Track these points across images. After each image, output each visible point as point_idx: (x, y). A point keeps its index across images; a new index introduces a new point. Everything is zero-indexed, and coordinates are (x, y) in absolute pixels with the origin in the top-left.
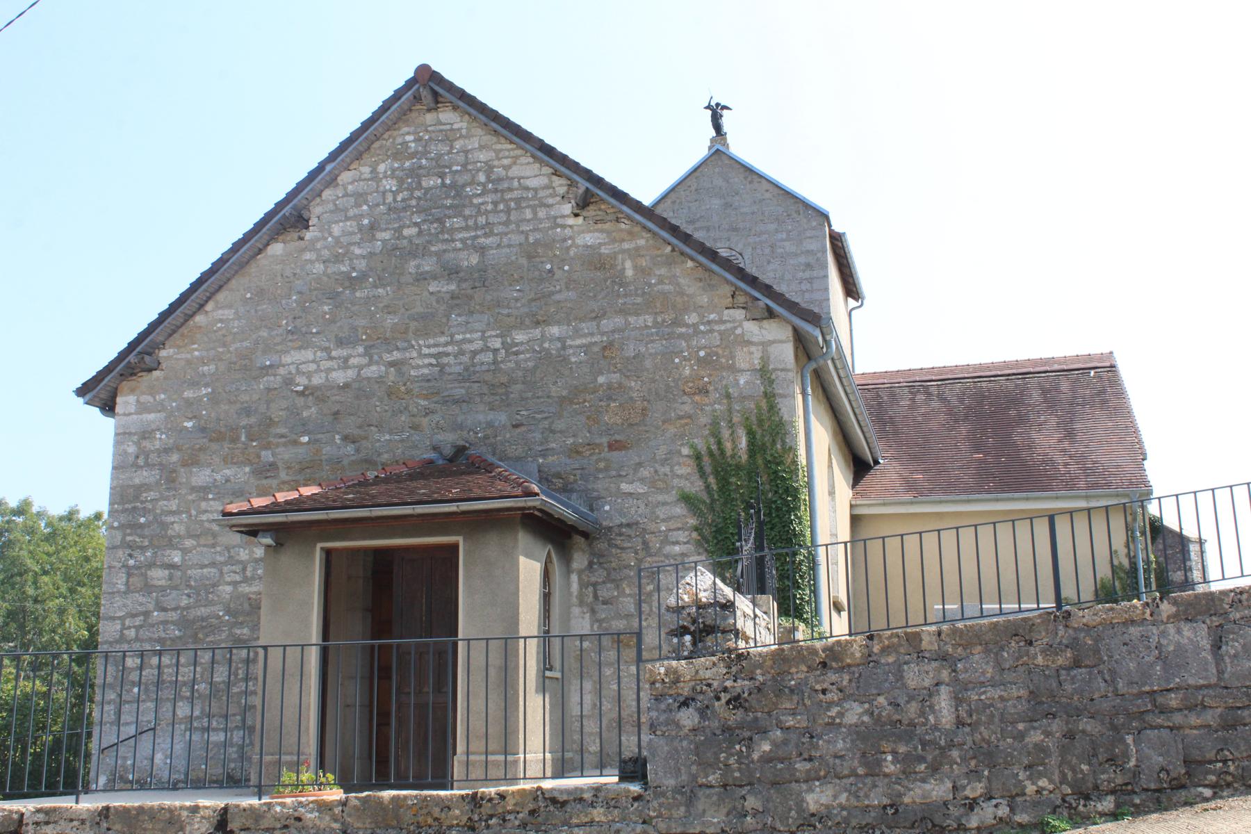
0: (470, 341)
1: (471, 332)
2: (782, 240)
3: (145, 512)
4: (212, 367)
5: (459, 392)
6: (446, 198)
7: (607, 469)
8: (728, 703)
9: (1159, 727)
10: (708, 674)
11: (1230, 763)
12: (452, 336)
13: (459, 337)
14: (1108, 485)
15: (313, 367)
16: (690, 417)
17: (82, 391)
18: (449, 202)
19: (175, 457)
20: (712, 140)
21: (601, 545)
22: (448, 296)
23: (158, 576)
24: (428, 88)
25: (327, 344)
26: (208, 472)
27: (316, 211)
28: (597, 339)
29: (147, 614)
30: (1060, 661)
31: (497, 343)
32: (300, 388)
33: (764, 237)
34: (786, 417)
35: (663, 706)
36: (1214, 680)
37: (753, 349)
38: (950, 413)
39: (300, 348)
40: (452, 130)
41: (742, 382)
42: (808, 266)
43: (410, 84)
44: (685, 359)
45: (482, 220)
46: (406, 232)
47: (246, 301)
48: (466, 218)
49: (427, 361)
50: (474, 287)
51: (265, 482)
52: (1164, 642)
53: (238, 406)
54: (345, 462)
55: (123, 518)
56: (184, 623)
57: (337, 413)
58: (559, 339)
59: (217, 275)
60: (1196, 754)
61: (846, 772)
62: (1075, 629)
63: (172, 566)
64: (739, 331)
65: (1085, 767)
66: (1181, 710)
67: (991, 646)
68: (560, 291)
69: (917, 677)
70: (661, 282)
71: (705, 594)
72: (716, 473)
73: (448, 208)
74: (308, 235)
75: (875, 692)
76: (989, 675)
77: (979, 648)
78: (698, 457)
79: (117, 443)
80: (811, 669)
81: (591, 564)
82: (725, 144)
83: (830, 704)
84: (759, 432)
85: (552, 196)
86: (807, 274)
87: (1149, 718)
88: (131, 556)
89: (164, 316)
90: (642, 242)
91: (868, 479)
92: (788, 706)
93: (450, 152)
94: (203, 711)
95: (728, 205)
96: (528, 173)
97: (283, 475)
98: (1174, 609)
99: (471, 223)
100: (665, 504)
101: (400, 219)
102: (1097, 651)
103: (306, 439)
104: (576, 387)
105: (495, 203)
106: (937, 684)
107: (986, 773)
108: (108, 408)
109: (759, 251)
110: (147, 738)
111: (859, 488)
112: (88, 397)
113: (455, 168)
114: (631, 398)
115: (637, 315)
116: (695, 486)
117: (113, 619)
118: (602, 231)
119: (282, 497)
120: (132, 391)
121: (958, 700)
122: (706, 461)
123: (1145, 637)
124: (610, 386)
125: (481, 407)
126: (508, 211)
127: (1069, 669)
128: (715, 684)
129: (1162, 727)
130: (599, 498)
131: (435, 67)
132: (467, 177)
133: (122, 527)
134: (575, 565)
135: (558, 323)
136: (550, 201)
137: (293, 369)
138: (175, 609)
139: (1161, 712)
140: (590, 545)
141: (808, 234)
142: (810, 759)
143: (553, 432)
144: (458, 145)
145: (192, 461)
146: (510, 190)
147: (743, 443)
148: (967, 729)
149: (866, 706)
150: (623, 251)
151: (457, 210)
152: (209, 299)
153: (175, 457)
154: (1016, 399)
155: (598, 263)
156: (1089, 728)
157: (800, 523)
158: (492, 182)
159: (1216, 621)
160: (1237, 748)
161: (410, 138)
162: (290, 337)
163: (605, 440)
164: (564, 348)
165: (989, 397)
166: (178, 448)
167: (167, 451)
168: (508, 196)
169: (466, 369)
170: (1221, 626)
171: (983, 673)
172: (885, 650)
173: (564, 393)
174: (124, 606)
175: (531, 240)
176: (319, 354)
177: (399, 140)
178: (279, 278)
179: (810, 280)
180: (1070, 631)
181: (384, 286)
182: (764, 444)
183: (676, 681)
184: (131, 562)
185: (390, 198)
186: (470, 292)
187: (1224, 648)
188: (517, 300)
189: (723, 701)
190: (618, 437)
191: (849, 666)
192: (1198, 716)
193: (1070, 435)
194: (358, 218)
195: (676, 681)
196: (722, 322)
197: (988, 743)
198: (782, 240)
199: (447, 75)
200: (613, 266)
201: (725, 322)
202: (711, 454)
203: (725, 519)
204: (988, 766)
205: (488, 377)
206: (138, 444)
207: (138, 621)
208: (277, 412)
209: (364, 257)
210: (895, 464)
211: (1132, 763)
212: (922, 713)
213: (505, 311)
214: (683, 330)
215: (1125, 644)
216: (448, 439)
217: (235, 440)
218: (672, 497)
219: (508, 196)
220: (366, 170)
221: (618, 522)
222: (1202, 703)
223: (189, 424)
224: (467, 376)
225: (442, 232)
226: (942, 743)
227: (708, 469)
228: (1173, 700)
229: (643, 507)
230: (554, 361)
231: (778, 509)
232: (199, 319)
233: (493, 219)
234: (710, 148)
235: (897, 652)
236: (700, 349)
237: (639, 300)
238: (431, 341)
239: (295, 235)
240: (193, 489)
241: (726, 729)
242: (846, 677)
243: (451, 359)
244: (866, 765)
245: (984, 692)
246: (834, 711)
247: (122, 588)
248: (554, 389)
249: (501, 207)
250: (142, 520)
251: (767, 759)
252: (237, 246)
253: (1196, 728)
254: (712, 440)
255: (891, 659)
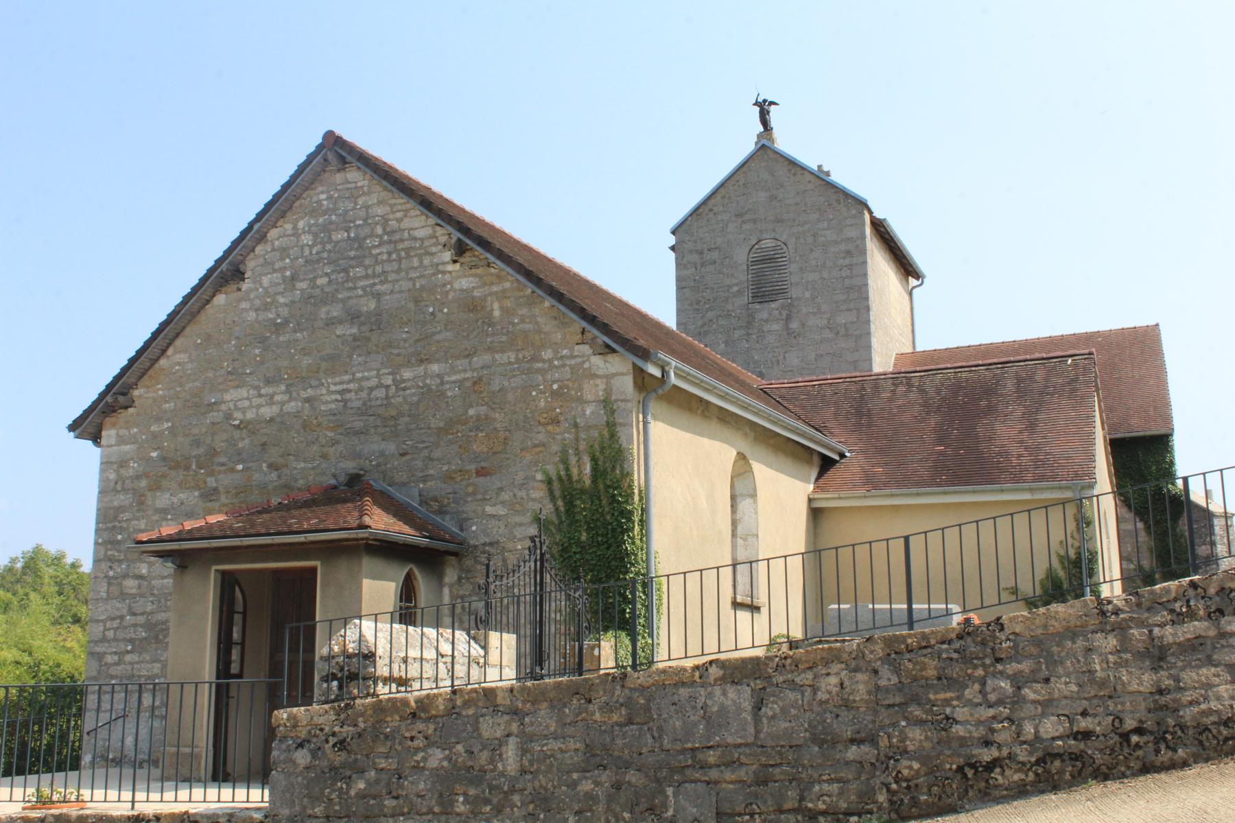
0: (368, 379)
1: (368, 371)
2: (824, 229)
3: (122, 530)
4: (172, 404)
5: (359, 425)
6: (351, 250)
7: (474, 493)
8: (334, 746)
9: (695, 781)
10: (321, 720)
11: (757, 816)
12: (354, 374)
13: (359, 375)
14: (1053, 478)
15: (246, 403)
16: (544, 445)
17: (73, 427)
18: (352, 254)
19: (144, 483)
20: (760, 136)
21: (468, 562)
22: (351, 339)
23: (130, 585)
24: (336, 152)
25: (257, 383)
26: (167, 496)
27: (251, 265)
28: (468, 375)
29: (122, 618)
30: (615, 717)
31: (388, 380)
32: (237, 422)
33: (807, 227)
34: (624, 445)
35: (284, 747)
36: (751, 740)
37: (598, 381)
38: (925, 405)
39: (237, 387)
40: (356, 188)
41: (588, 412)
42: (848, 253)
43: (320, 148)
44: (541, 392)
45: (379, 269)
46: (320, 282)
47: (197, 346)
48: (366, 268)
49: (334, 397)
50: (372, 329)
51: (210, 504)
52: (709, 702)
53: (191, 438)
54: (270, 487)
55: (106, 535)
56: (149, 626)
57: (264, 444)
58: (438, 376)
59: (172, 325)
60: (726, 807)
61: (424, 810)
62: (631, 689)
63: (141, 577)
64: (586, 365)
65: (626, 815)
66: (719, 766)
67: (555, 703)
68: (439, 332)
69: (490, 728)
70: (522, 321)
71: (352, 645)
72: (564, 498)
73: (352, 259)
74: (245, 286)
75: (453, 740)
76: (552, 729)
77: (545, 705)
78: (549, 482)
79: (102, 471)
80: (402, 719)
81: (460, 579)
82: (772, 140)
83: (417, 750)
84: (602, 458)
85: (435, 245)
86: (847, 261)
87: (688, 772)
88: (111, 567)
89: (132, 361)
90: (507, 285)
91: (831, 473)
92: (382, 749)
93: (354, 209)
94: (162, 703)
95: (773, 198)
96: (417, 225)
97: (223, 499)
98: (721, 672)
99: (370, 272)
100: (521, 525)
101: (314, 270)
102: (648, 709)
103: (240, 467)
104: (451, 419)
105: (389, 254)
106: (508, 736)
107: (542, 816)
108: (96, 439)
109: (802, 241)
110: (120, 721)
111: (821, 481)
112: (78, 431)
113: (358, 222)
114: (495, 429)
115: (502, 352)
116: (548, 510)
117: (98, 621)
118: (475, 275)
119: (189, 525)
120: (114, 425)
121: (524, 751)
122: (556, 485)
123: (692, 698)
124: (478, 418)
125: (376, 438)
126: (400, 260)
127: (621, 725)
128: (327, 729)
129: (700, 781)
130: (467, 519)
131: (338, 132)
132: (367, 231)
133: (104, 543)
134: (447, 580)
135: (438, 361)
136: (434, 249)
137: (231, 405)
138: (142, 614)
139: (702, 768)
140: (460, 561)
141: (848, 222)
142: (397, 798)
143: (432, 460)
144: (360, 201)
145: (156, 487)
146: (402, 240)
147: (588, 469)
148: (529, 777)
149: (447, 752)
150: (491, 294)
151: (359, 261)
152: (169, 345)
153: (144, 483)
154: (990, 390)
155: (472, 305)
156: (634, 780)
157: (633, 543)
158: (387, 233)
159: (759, 684)
160: (765, 802)
161: (323, 196)
162: (230, 377)
163: (473, 467)
164: (442, 383)
165: (965, 388)
166: (146, 475)
167: (138, 477)
168: (400, 246)
169: (364, 404)
170: (764, 688)
171: (547, 727)
172: (466, 704)
173: (442, 424)
174: (106, 610)
175: (418, 286)
176: (251, 392)
177: (315, 199)
178: (222, 325)
179: (850, 267)
180: (627, 691)
181: (301, 331)
182: (605, 470)
183: (295, 726)
184: (111, 573)
185: (307, 252)
186: (368, 334)
187: (763, 709)
188: (405, 341)
189: (331, 743)
190: (484, 464)
191: (436, 716)
192: (733, 772)
193: (1031, 427)
194: (284, 269)
195: (295, 726)
196: (572, 357)
197: (546, 789)
198: (824, 229)
199: (348, 137)
200: (483, 308)
201: (575, 357)
202: (560, 479)
203: (570, 539)
204: (543, 810)
205: (381, 411)
206: (117, 471)
207: (116, 624)
208: (220, 445)
209: (286, 305)
210: (860, 457)
211: (670, 813)
212: (492, 761)
213: (396, 351)
214: (540, 365)
215: (674, 704)
216: (350, 466)
217: (187, 468)
218: (528, 518)
219: (400, 246)
220: (289, 227)
221: (482, 541)
222: (738, 759)
223: (154, 454)
224: (364, 411)
225: (347, 281)
226: (506, 788)
227: (557, 493)
228: (712, 757)
229: (503, 528)
230: (432, 395)
231: (614, 530)
232: (163, 362)
233: (388, 268)
234: (756, 143)
235: (477, 706)
236: (554, 382)
237: (504, 338)
238: (337, 379)
239: (234, 287)
240: (157, 511)
241: (333, 768)
242: (432, 727)
243: (352, 396)
244: (441, 803)
245: (546, 744)
246: (419, 757)
247: (104, 595)
248: (433, 420)
249: (394, 256)
250: (119, 537)
251: (362, 796)
252: (187, 299)
253: (731, 782)
254: (561, 467)
255: (471, 712)
